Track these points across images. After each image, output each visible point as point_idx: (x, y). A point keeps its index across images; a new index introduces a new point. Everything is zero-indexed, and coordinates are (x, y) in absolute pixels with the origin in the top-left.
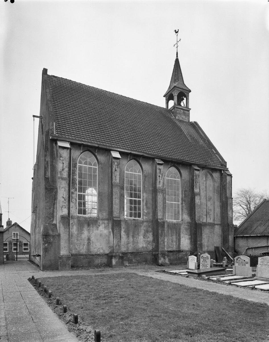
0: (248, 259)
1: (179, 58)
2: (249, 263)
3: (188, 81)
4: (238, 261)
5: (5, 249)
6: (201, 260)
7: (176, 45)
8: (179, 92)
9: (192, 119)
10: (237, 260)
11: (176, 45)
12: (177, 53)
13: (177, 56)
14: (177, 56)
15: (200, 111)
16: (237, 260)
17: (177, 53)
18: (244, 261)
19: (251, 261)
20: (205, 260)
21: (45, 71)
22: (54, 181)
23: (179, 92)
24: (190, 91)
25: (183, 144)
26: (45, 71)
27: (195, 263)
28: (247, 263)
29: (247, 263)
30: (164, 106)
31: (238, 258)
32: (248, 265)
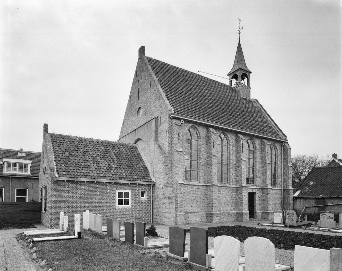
0: (332, 216)
1: (241, 43)
2: (333, 218)
3: (250, 65)
4: (323, 217)
5: (126, 236)
6: (287, 216)
7: (239, 32)
8: (241, 73)
9: (253, 96)
10: (322, 216)
11: (239, 32)
12: (239, 38)
13: (239, 42)
14: (239, 42)
15: (261, 90)
16: (322, 216)
17: (239, 38)
18: (329, 216)
19: (335, 217)
20: (290, 215)
21: (142, 50)
22: (285, 219)
23: (241, 73)
24: (251, 72)
25: (180, 100)
26: (142, 50)
27: (281, 218)
28: (331, 218)
29: (331, 218)
30: (227, 83)
31: (323, 214)
32: (332, 220)
